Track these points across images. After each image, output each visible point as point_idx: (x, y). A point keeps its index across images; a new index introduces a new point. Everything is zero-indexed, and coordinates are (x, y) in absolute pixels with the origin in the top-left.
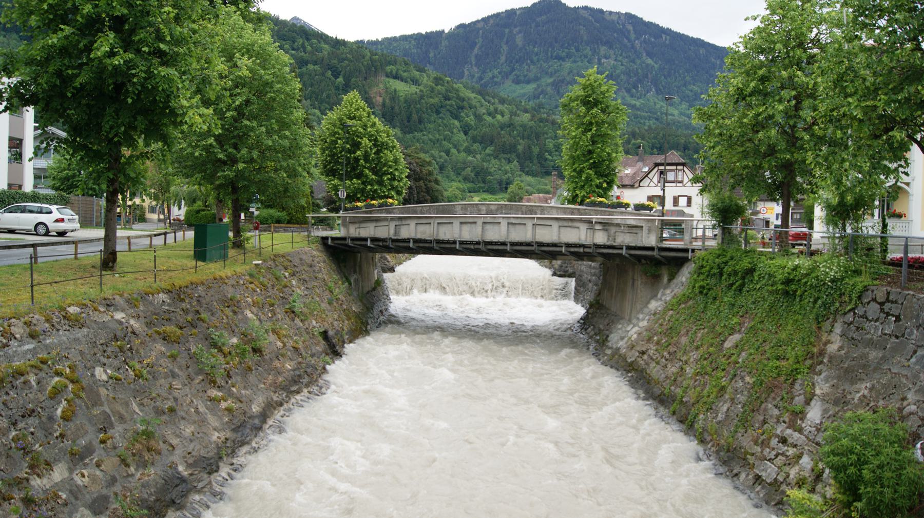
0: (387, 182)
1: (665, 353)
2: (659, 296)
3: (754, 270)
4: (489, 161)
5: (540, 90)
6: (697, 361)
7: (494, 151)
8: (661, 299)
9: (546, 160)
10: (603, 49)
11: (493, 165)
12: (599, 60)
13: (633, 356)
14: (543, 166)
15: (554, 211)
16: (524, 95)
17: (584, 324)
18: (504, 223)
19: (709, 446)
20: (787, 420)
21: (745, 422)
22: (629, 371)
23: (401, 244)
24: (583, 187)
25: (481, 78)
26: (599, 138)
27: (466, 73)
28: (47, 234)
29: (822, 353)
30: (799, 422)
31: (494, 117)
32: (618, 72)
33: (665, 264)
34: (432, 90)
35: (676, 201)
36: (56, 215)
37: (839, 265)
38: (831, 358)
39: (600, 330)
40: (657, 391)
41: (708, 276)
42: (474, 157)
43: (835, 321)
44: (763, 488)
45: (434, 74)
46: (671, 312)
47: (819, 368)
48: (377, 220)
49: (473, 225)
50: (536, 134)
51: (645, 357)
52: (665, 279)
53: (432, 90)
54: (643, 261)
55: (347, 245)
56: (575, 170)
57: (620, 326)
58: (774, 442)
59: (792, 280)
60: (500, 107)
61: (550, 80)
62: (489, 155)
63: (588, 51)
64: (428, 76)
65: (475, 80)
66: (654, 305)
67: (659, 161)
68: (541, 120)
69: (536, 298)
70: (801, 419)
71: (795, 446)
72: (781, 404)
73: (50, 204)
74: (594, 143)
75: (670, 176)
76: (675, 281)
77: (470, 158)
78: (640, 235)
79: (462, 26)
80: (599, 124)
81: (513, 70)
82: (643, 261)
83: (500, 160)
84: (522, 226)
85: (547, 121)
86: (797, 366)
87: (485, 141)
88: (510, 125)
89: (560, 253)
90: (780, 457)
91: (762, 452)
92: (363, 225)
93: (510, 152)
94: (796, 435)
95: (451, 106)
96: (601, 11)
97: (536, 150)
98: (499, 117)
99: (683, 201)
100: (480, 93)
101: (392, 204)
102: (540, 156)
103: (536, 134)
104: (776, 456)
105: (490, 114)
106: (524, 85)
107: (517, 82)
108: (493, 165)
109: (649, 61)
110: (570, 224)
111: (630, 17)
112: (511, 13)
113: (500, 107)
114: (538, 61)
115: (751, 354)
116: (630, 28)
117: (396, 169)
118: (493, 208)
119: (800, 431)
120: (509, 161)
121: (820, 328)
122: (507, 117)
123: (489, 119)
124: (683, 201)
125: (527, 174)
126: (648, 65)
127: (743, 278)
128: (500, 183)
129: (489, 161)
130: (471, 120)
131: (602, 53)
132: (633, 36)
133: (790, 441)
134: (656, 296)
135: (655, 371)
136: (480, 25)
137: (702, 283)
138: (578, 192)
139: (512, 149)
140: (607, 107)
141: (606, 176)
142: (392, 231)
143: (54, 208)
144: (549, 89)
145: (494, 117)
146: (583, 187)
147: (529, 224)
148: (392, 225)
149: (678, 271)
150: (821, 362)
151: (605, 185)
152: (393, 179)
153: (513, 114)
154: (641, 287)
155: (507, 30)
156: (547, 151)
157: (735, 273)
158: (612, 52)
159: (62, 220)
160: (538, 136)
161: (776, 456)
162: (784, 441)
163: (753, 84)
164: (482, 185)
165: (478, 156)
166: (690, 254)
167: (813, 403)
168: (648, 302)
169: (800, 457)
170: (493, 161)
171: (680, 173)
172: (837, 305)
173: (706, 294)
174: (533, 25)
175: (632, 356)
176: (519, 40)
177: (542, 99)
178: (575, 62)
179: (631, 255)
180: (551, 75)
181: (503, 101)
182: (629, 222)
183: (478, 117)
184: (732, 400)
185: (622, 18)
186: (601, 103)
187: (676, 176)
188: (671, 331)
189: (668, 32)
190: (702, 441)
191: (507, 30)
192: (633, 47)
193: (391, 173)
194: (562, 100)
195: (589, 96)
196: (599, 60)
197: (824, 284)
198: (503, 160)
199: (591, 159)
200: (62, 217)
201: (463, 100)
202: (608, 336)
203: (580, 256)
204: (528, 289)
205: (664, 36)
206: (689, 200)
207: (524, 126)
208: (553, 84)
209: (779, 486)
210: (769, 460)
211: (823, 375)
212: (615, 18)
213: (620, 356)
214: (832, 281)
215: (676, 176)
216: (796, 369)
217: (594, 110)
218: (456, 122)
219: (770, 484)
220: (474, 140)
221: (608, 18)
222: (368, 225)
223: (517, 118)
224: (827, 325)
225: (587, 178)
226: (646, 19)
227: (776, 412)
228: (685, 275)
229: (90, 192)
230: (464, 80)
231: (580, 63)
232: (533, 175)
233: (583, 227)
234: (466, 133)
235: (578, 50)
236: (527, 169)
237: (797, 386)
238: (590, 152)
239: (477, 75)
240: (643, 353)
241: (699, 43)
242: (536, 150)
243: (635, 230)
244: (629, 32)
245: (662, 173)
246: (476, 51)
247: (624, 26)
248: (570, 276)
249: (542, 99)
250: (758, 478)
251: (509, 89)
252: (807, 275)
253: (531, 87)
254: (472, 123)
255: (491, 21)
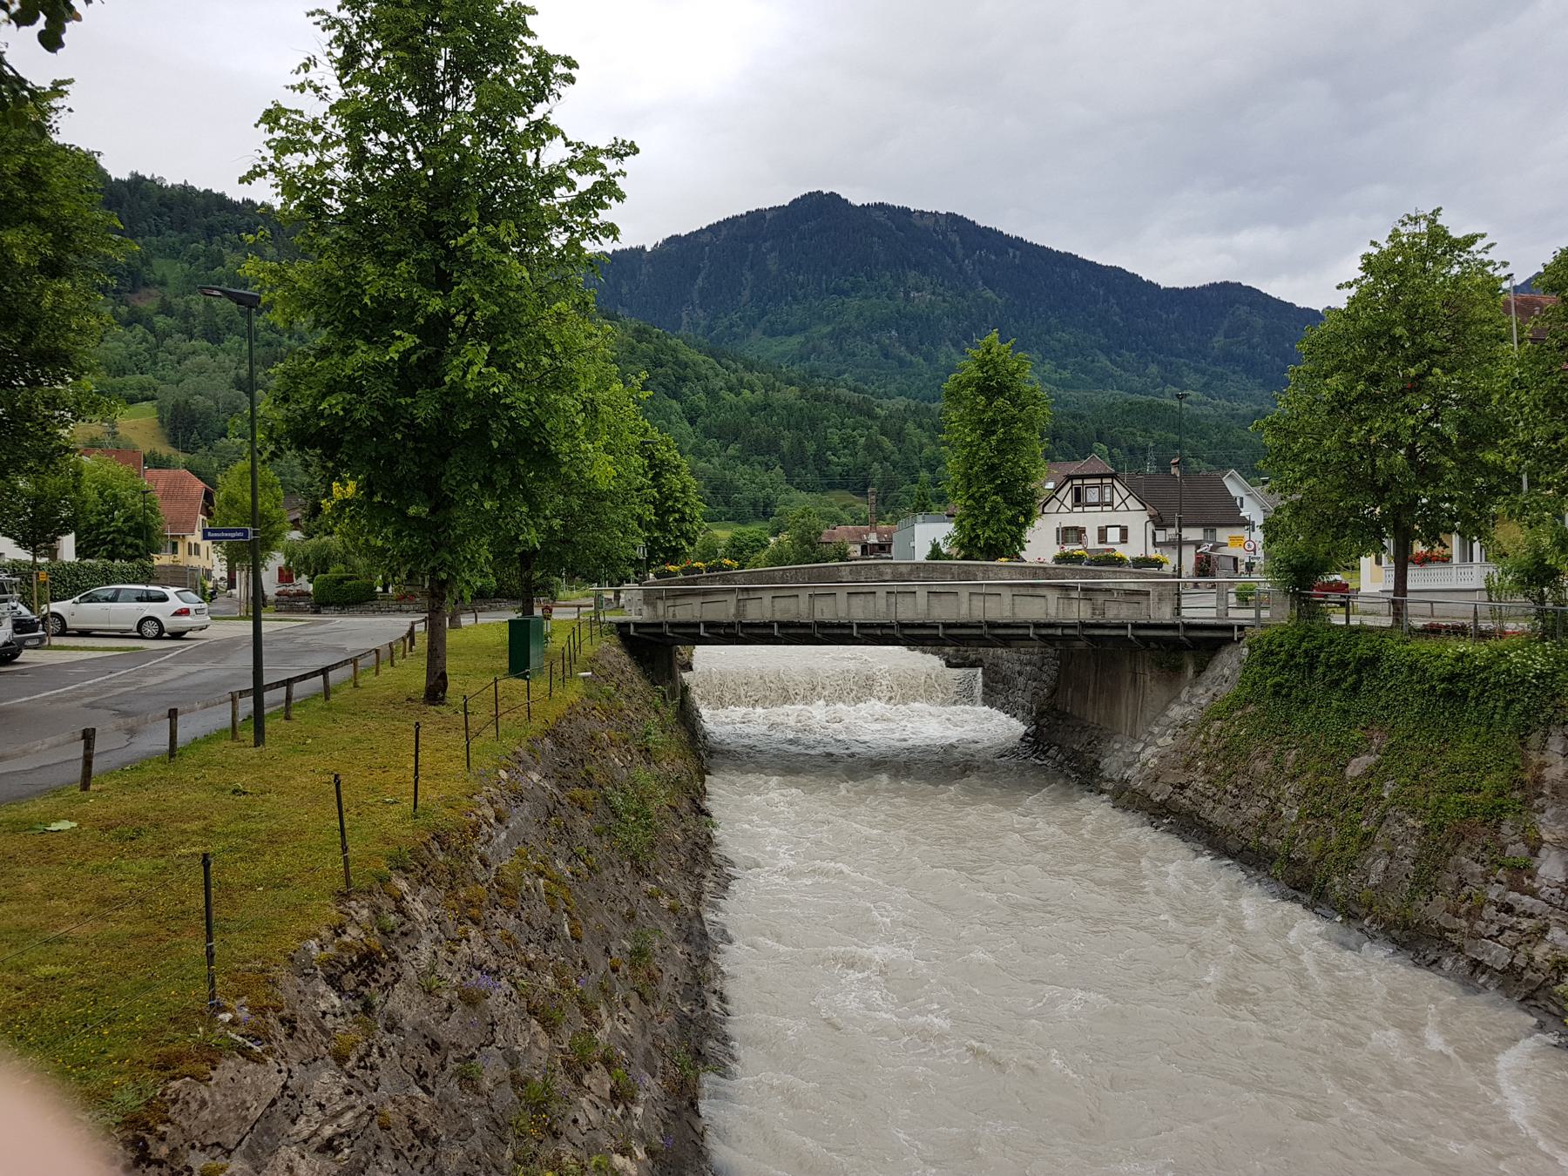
0: (673, 526)
1: (1229, 787)
2: (1184, 696)
3: (1378, 659)
4: (733, 468)
5: (810, 345)
6: (1299, 798)
7: (742, 451)
8: (1190, 702)
9: (828, 463)
10: (912, 276)
11: (741, 476)
12: (907, 294)
13: (1162, 791)
14: (823, 474)
15: (1005, 573)
16: (784, 354)
17: (1037, 742)
18: (922, 595)
19: (1366, 922)
20: (1504, 879)
21: (1424, 884)
22: (1162, 816)
23: (756, 631)
24: (986, 523)
25: (711, 329)
26: (1011, 444)
27: (685, 319)
28: (159, 637)
29: (1538, 781)
30: (1527, 881)
31: (738, 394)
32: (938, 312)
33: (1188, 649)
34: (633, 351)
35: (1102, 534)
36: (175, 603)
37: (1545, 653)
38: (1556, 790)
39: (1074, 751)
40: (1234, 846)
41: (1283, 668)
42: (709, 461)
43: (1547, 734)
44: (1491, 978)
45: (634, 323)
46: (1218, 723)
47: (1537, 802)
48: (706, 593)
49: (870, 597)
50: (810, 419)
51: (1189, 793)
52: (1190, 672)
53: (633, 351)
54: (1152, 645)
55: (663, 635)
56: (971, 497)
57: (1117, 746)
58: (1490, 912)
59: (1459, 675)
60: (747, 376)
61: (827, 329)
62: (733, 458)
63: (887, 279)
64: (624, 327)
65: (699, 331)
66: (1176, 712)
67: (1072, 472)
68: (817, 397)
69: (911, 703)
70: (1529, 877)
71: (1531, 916)
72: (1485, 856)
73: (163, 585)
74: (1002, 452)
75: (1092, 495)
76: (1208, 673)
77: (702, 464)
78: (1144, 606)
79: (674, 239)
80: (1009, 422)
81: (763, 313)
82: (1152, 645)
83: (751, 465)
84: (952, 597)
85: (826, 398)
86: (1499, 801)
87: (727, 434)
88: (766, 406)
89: (1026, 638)
90: (1507, 933)
91: (1471, 926)
92: (679, 602)
93: (768, 453)
94: (1526, 899)
95: (666, 376)
96: (906, 211)
97: (811, 447)
98: (746, 393)
99: (1114, 535)
100: (711, 354)
101: (730, 568)
102: (819, 458)
103: (810, 419)
104: (1501, 931)
105: (731, 389)
106: (785, 338)
107: (772, 333)
108: (741, 476)
109: (989, 294)
110: (1031, 591)
111: (951, 217)
112: (756, 217)
113: (747, 376)
114: (805, 297)
115: (1405, 785)
116: (956, 238)
117: (686, 504)
118: (903, 569)
119: (1533, 894)
120: (768, 468)
121: (1523, 745)
122: (760, 393)
123: (730, 397)
124: (1114, 535)
125: (799, 487)
126: (986, 300)
127: (1358, 671)
128: (754, 504)
129: (733, 468)
130: (701, 400)
131: (911, 282)
132: (960, 252)
133: (1518, 908)
134: (1178, 696)
135: (1218, 815)
136: (706, 238)
137: (1277, 679)
138: (979, 532)
139: (772, 446)
140: (1019, 394)
141: (1019, 504)
142: (732, 611)
143: (170, 591)
144: (825, 344)
145: (738, 394)
146: (986, 523)
147: (964, 594)
148: (732, 600)
149: (1211, 658)
150: (1541, 795)
151: (1022, 519)
152: (683, 519)
153: (769, 388)
154: (1153, 690)
155: (751, 246)
156: (829, 449)
157: (1343, 664)
158: (927, 280)
159: (186, 612)
160: (813, 423)
161: (1501, 931)
162: (1509, 909)
163: (1360, 387)
164: (725, 509)
165: (715, 460)
166: (1236, 634)
167: (1543, 853)
168: (1166, 708)
169: (1545, 930)
170: (741, 468)
171: (1108, 490)
172: (1550, 710)
173: (1288, 695)
174: (794, 237)
175: (1160, 793)
176: (772, 264)
177: (814, 362)
178: (866, 297)
179: (1137, 637)
180: (828, 321)
181: (750, 367)
182: (1126, 587)
183: (712, 395)
184: (1391, 854)
185: (942, 222)
186: (1008, 388)
187: (1101, 494)
188: (1230, 751)
189: (1018, 243)
190: (1350, 917)
191: (751, 246)
192: (960, 269)
193: (678, 511)
194: (945, 386)
195: (990, 378)
196: (907, 294)
197: (1523, 682)
198: (757, 467)
199: (996, 478)
200: (185, 606)
201: (686, 366)
202: (1097, 762)
203: (1006, 641)
204: (905, 691)
205: (1011, 251)
206: (1124, 532)
207: (788, 407)
208: (831, 335)
209: (1521, 974)
210: (1490, 938)
211: (1549, 813)
212: (930, 223)
213: (1134, 791)
214: (1537, 677)
215: (1101, 494)
216: (1501, 806)
217: (999, 402)
218: (676, 405)
219: (1503, 972)
220: (707, 433)
221: (919, 223)
222: (689, 600)
223: (778, 395)
224: (1534, 740)
225: (993, 509)
226: (981, 223)
227: (1478, 868)
228: (1229, 664)
229: (130, 552)
230: (682, 332)
231: (874, 300)
232: (810, 491)
233: (1052, 595)
234: (692, 422)
235: (870, 278)
236: (798, 480)
237: (1505, 829)
238: (993, 468)
239: (703, 323)
240: (1182, 787)
241: (1070, 261)
242: (811, 447)
243: (1136, 599)
244: (954, 245)
245: (1078, 491)
246: (699, 281)
247: (945, 235)
248: (973, 665)
249: (814, 362)
250: (1476, 965)
251: (758, 346)
252: (1485, 668)
253: (794, 342)
254: (703, 405)
255: (724, 232)
